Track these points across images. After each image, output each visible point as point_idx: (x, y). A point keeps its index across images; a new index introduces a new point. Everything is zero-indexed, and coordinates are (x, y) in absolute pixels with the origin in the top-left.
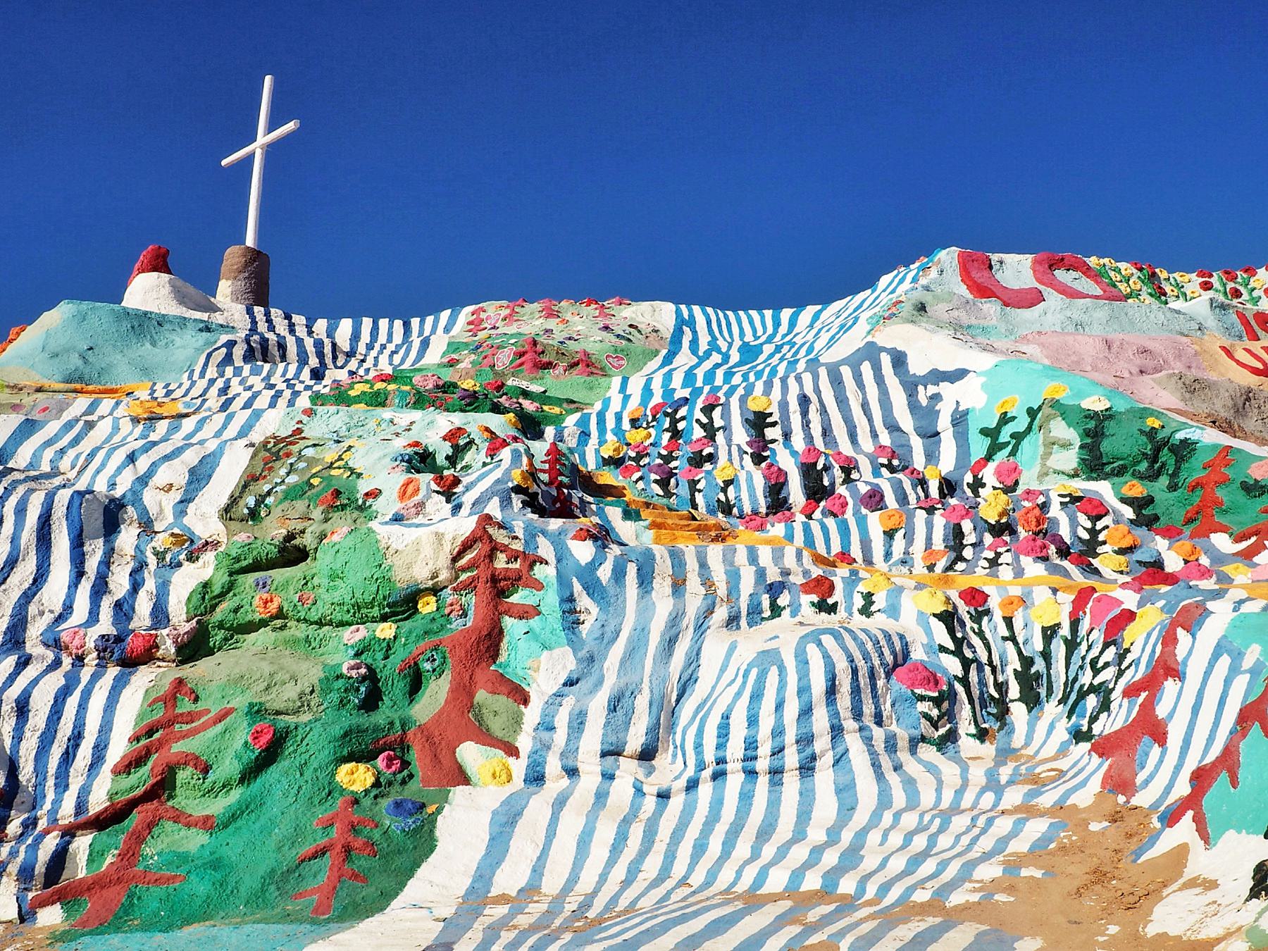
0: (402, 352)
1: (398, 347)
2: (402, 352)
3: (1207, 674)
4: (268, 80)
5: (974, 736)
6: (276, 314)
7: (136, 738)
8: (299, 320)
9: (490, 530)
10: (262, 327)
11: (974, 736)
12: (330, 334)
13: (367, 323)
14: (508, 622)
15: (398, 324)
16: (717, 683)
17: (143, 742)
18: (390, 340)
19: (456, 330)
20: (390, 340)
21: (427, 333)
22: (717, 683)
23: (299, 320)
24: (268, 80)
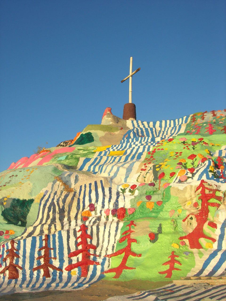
0: (174, 130)
1: (173, 128)
2: (174, 130)
3: (104, 235)
4: (131, 58)
5: (7, 224)
6: (140, 122)
7: (123, 234)
8: (145, 123)
9: (203, 183)
10: (136, 126)
11: (7, 224)
12: (154, 126)
13: (164, 122)
14: (210, 208)
15: (172, 121)
16: (115, 241)
17: (125, 235)
18: (170, 126)
19: (189, 121)
20: (170, 126)
21: (180, 124)
22: (115, 241)
23: (145, 123)
24: (131, 58)
